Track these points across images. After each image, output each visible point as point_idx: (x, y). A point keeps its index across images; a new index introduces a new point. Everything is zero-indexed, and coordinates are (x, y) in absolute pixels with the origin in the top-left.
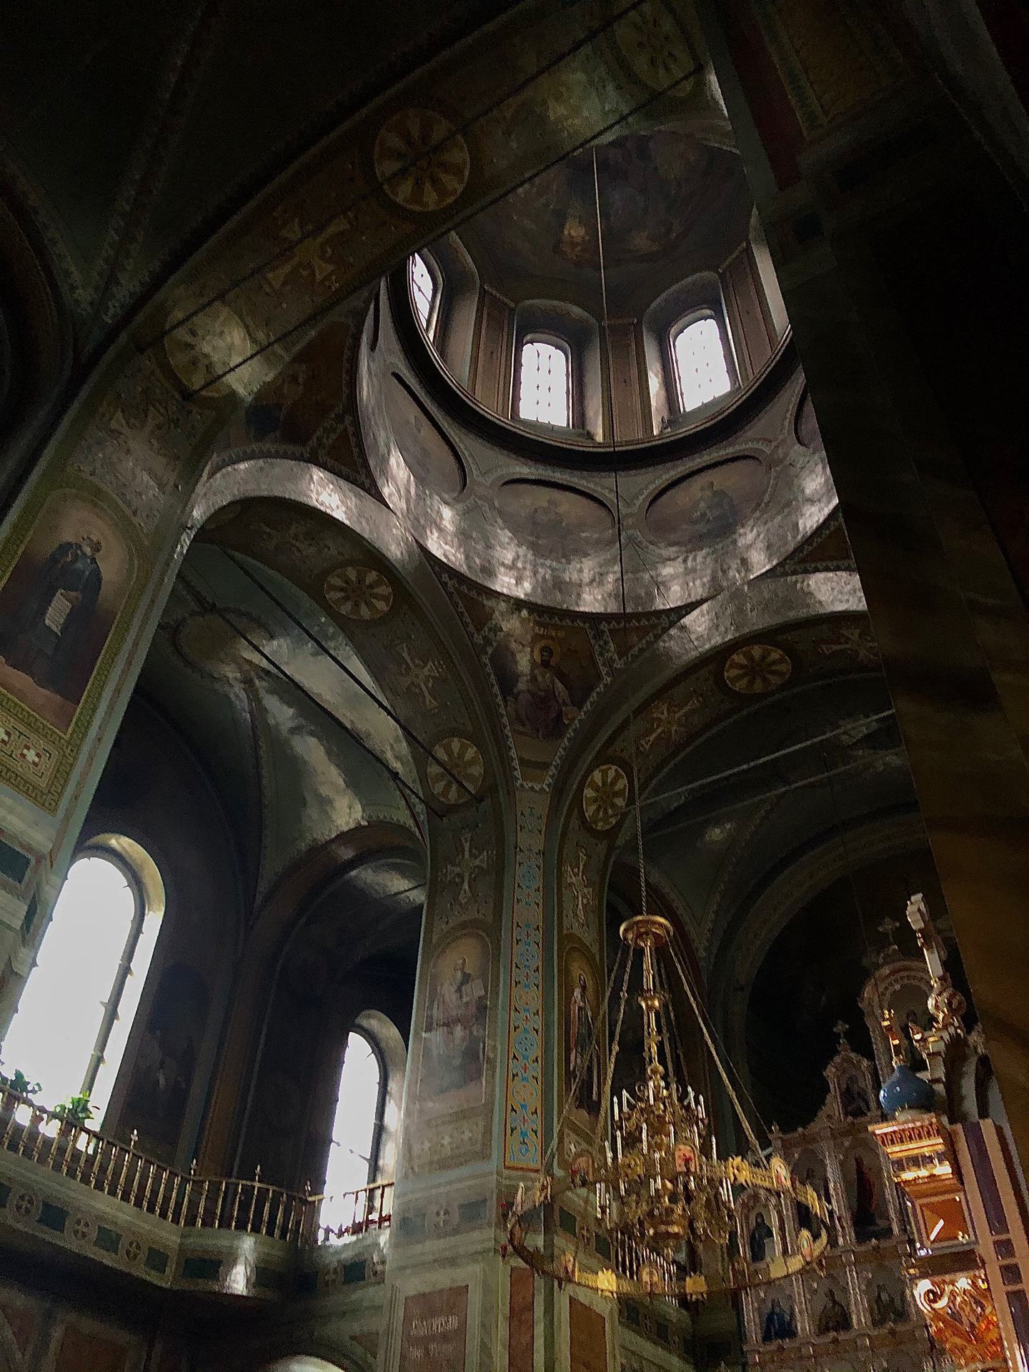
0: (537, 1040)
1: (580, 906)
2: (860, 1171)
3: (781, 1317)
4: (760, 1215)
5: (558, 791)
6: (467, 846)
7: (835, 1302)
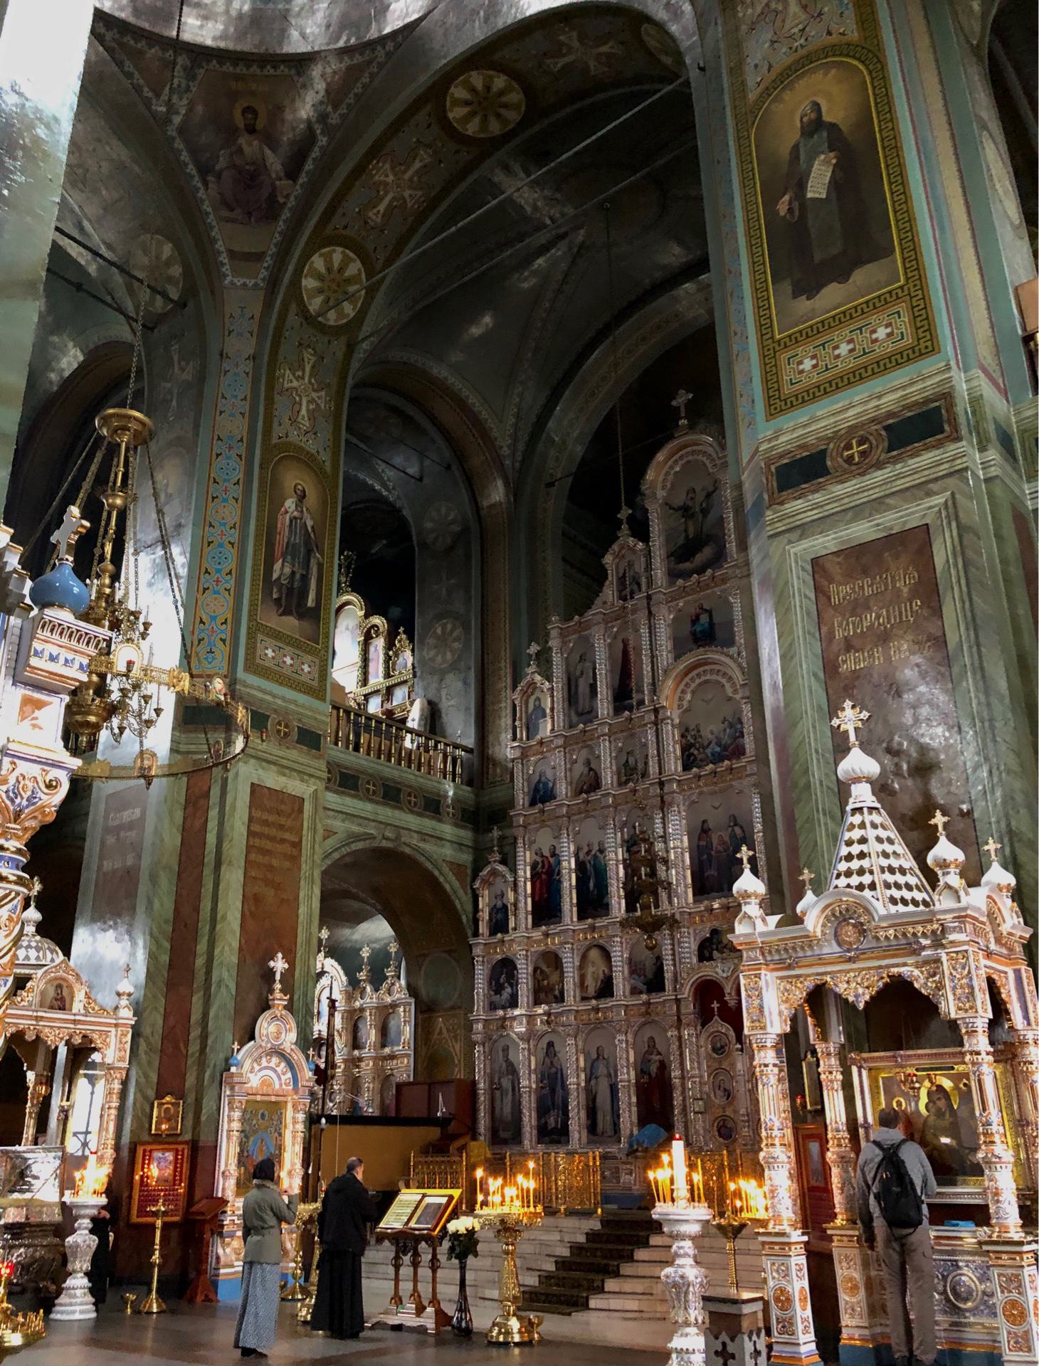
0: (232, 553)
1: (304, 412)
2: (625, 653)
3: (546, 784)
4: (538, 699)
5: (273, 283)
6: (176, 358)
7: (591, 769)
